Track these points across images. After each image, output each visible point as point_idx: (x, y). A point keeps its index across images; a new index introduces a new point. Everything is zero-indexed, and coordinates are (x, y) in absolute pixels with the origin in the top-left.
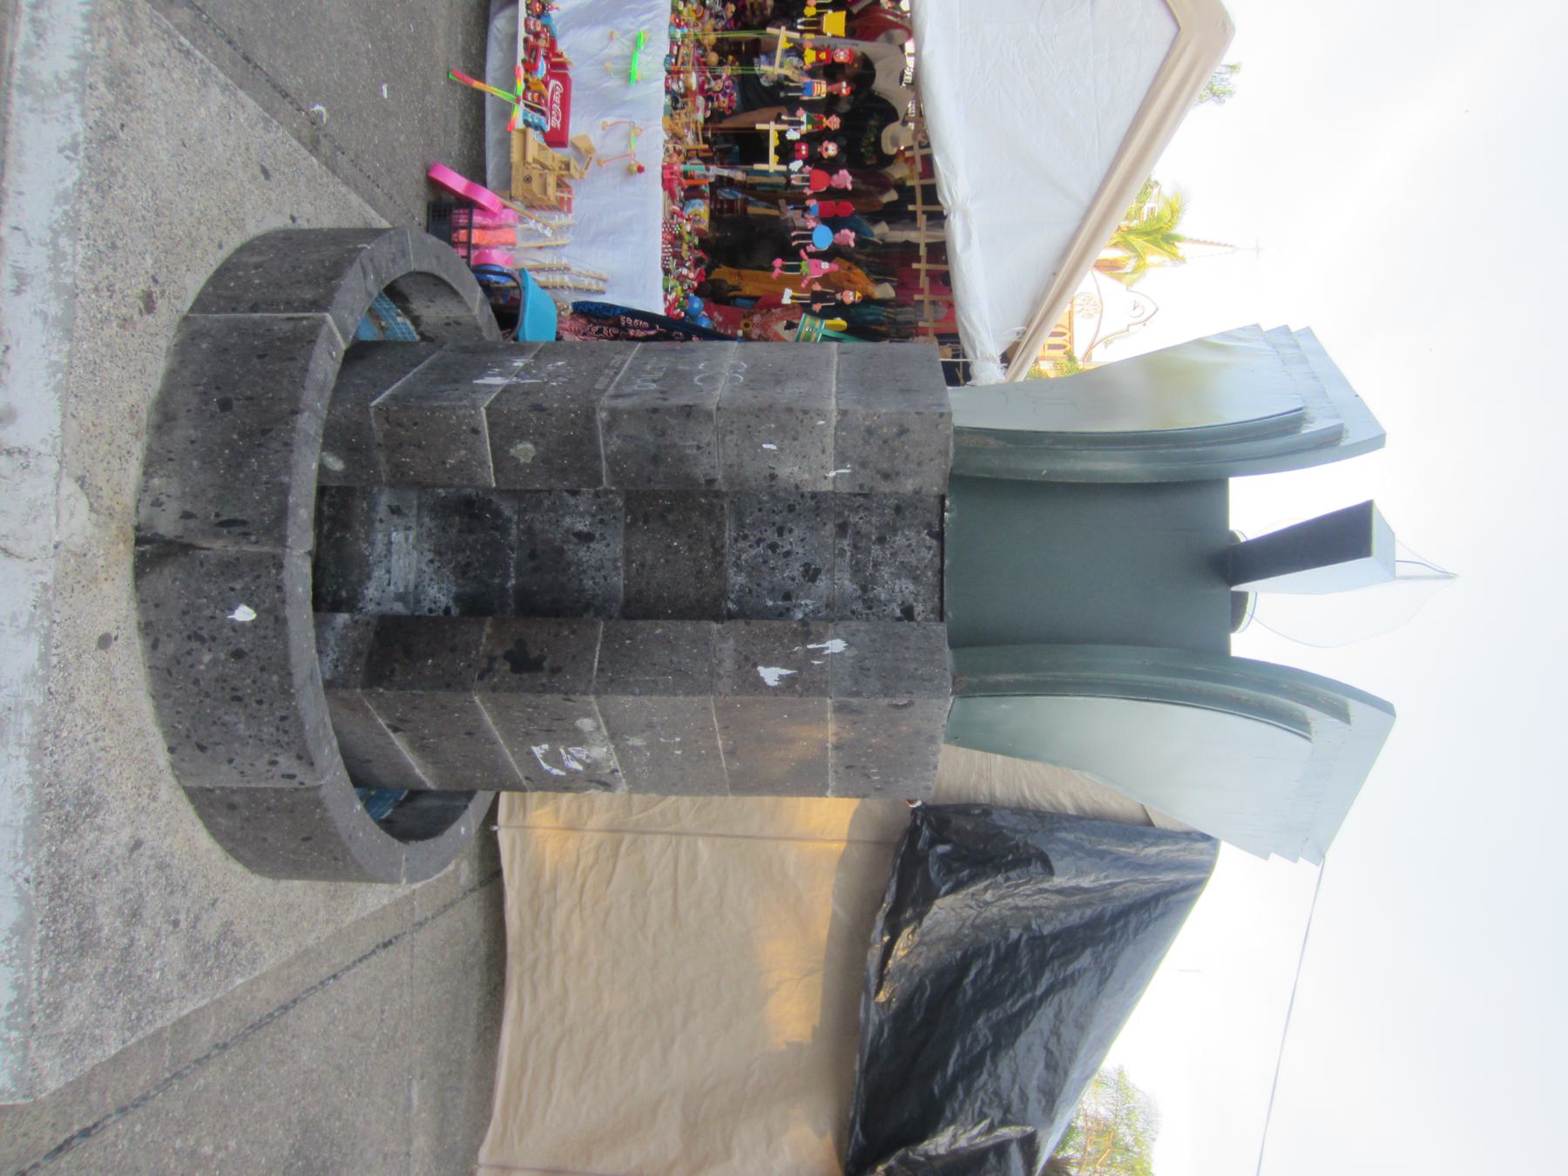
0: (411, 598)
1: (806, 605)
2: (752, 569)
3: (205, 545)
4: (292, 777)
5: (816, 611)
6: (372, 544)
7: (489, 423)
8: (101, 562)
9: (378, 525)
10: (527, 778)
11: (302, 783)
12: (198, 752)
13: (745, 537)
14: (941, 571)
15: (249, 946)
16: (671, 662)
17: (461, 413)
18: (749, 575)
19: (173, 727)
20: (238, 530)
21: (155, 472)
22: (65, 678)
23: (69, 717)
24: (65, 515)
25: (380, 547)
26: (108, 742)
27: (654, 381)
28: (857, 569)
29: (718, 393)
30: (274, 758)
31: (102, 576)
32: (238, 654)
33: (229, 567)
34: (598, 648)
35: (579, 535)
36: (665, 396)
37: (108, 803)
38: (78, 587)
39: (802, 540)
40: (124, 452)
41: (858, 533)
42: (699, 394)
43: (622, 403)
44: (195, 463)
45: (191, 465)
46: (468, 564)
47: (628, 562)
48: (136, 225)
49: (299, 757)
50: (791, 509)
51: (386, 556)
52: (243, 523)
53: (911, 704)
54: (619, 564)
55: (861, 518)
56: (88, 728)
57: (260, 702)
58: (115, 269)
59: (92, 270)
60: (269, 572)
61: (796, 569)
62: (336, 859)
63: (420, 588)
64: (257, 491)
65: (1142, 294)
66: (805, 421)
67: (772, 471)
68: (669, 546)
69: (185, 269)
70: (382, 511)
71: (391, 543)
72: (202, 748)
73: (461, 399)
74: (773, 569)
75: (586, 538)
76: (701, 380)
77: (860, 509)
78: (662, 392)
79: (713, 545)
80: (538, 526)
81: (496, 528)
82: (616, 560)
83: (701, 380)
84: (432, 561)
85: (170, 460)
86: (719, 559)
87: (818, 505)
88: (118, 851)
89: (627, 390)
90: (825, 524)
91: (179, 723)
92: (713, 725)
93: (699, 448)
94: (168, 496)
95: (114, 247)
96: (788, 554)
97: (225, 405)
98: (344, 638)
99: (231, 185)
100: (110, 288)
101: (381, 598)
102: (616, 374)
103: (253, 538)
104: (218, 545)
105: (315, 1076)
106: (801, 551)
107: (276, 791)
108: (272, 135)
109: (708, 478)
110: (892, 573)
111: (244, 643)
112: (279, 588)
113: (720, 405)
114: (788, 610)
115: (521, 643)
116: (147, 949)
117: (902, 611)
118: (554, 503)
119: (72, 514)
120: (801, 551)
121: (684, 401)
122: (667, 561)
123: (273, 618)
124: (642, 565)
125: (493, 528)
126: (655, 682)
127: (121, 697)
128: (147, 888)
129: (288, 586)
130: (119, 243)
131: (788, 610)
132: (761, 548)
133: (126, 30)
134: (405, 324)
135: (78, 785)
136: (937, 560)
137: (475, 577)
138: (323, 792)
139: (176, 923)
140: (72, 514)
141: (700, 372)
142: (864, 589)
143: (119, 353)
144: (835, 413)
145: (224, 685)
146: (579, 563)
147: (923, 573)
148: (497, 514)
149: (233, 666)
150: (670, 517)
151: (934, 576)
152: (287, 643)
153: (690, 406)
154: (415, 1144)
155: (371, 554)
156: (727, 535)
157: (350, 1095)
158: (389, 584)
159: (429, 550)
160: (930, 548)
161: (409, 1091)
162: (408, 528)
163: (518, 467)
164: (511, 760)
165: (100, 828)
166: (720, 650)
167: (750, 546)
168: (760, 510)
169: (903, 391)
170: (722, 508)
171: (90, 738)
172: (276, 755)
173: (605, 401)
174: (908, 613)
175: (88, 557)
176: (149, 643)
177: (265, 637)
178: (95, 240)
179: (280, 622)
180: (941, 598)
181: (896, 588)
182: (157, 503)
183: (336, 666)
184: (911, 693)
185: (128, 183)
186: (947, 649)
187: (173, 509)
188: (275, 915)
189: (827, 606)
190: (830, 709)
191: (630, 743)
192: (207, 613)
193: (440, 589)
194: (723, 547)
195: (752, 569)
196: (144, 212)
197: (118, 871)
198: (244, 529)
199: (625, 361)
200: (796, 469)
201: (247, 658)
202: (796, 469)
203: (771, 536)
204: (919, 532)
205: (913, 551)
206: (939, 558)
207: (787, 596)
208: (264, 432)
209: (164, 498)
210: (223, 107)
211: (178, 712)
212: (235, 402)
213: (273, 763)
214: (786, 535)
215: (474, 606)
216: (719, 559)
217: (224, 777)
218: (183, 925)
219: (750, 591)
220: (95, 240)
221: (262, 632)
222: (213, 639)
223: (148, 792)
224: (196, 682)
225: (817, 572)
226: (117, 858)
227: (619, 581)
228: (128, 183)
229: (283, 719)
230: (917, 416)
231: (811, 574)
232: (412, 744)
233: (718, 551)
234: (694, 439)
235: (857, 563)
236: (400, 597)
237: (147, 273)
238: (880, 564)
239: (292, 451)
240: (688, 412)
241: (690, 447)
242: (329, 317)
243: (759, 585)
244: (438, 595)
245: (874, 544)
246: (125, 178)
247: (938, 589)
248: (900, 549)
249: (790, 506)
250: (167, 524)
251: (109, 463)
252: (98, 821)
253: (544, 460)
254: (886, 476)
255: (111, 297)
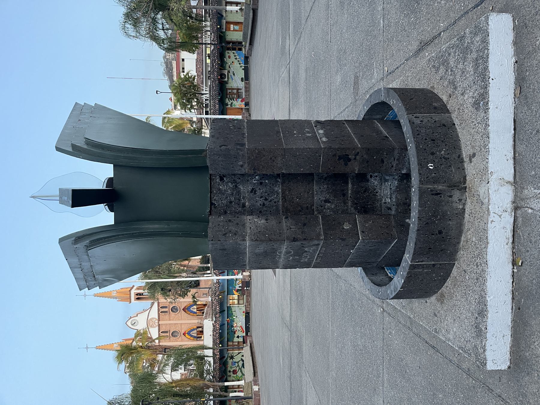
0: (383, 181)
1: (255, 181)
2: (273, 192)
3: (444, 187)
4: (415, 117)
5: (252, 179)
6: (396, 197)
7: (359, 235)
8: (476, 180)
9: (395, 204)
10: (344, 124)
11: (413, 115)
12: (446, 124)
13: (275, 202)
14: (211, 192)
15: (431, 66)
16: (298, 159)
17: (368, 237)
18: (274, 190)
19: (453, 131)
20: (434, 192)
21: (462, 210)
22: (484, 142)
23: (483, 131)
24: (486, 192)
25: (394, 197)
26: (471, 124)
27: (306, 251)
28: (239, 193)
29: (285, 247)
30: (421, 123)
31: (475, 176)
32: (433, 154)
33: (436, 181)
34: (321, 163)
35: (329, 202)
36: (302, 245)
37: (471, 106)
38: (482, 171)
39: (257, 202)
40: (471, 215)
41: (238, 204)
42: (291, 246)
43: (316, 242)
44: (449, 213)
45: (450, 213)
46: (365, 192)
47: (313, 193)
48: (471, 288)
49: (413, 123)
50: (261, 212)
51: (392, 194)
52: (433, 194)
53: (220, 146)
54: (316, 193)
55: (238, 209)
56: (477, 128)
57: (426, 139)
58: (476, 272)
59: (483, 270)
60: (424, 179)
61: (258, 193)
62: (403, 94)
63: (380, 184)
64: (429, 205)
65: (129, 327)
66: (256, 237)
67: (267, 221)
68: (300, 199)
69: (457, 278)
70: (394, 208)
71: (390, 198)
72: (444, 125)
73: (368, 242)
74: (266, 192)
75: (327, 201)
76: (291, 252)
77: (238, 212)
78: (303, 247)
79: (286, 199)
80: (342, 204)
81: (356, 204)
82: (317, 194)
83: (291, 252)
84: (377, 193)
85: (457, 214)
86: (283, 195)
87: (251, 213)
88: (468, 91)
89: (314, 248)
90: (249, 207)
91: (451, 133)
92: (284, 140)
93: (291, 228)
94: (457, 202)
95: (477, 279)
96: (261, 197)
97: (440, 232)
98: (403, 165)
99: (445, 308)
100: (477, 266)
101: (393, 180)
102: (318, 254)
103: (429, 190)
104: (440, 187)
105: (412, 28)
106: (257, 198)
107: (421, 113)
108: (434, 328)
109: (288, 219)
110: (227, 192)
111: (431, 157)
112: (420, 174)
113: (284, 242)
114: (261, 179)
115: (346, 164)
116: (459, 62)
117: (224, 179)
118: (337, 212)
119: (484, 193)
120: (257, 198)
121: (296, 243)
122: (300, 194)
123: (422, 165)
124: (308, 193)
125: (357, 204)
126: (303, 152)
127: (469, 139)
128: (460, 81)
129: (418, 175)
130: (476, 281)
131: (261, 179)
132: (270, 199)
133: (478, 349)
134: (390, 274)
135: (480, 110)
136: (212, 196)
137: (362, 188)
138: (406, 113)
139: (451, 71)
140: (484, 193)
141: (291, 256)
142: (236, 186)
143: (474, 246)
144: (247, 240)
145: (437, 144)
146: (328, 193)
147: (217, 192)
148: (356, 209)
149: (434, 150)
150: (300, 208)
151: (213, 191)
152: (417, 158)
153: (294, 241)
154: (381, 7)
155: (397, 194)
156: (281, 204)
157: (402, 22)
158: (390, 185)
159: (377, 196)
160: (215, 200)
161: (383, 24)
162: (385, 203)
163: (349, 221)
164: (349, 129)
165: (473, 97)
166: (282, 164)
167: (273, 199)
168: (271, 211)
169: (225, 250)
170: (283, 212)
171: (477, 125)
172: (421, 124)
173: (322, 243)
174: (222, 179)
175: (479, 181)
176: (461, 157)
177: (425, 159)
178: (482, 280)
179: (420, 164)
180: (211, 184)
181: (226, 187)
182: (460, 200)
183: (405, 155)
184: (220, 150)
185: (474, 300)
186: (208, 164)
187: (455, 198)
188: (423, 77)
189: (248, 181)
190: (246, 145)
191: (311, 134)
192: (443, 166)
193: (374, 183)
194: (282, 199)
195: (273, 192)
196: (469, 292)
197: (468, 85)
198: (432, 192)
199: (316, 260)
200: (259, 222)
201: (430, 153)
202: (259, 222)
203: (267, 203)
204: (219, 205)
205: (220, 199)
206: (212, 197)
207: (261, 183)
208: (427, 223)
209: (458, 202)
210: (449, 333)
211: (452, 136)
212: (437, 233)
213: (421, 121)
214: (262, 204)
215: (362, 177)
216: (283, 195)
217: (436, 117)
218: (449, 70)
219: (273, 185)
220: (482, 280)
221: (425, 160)
222: (441, 158)
223: (461, 111)
224: (446, 145)
225: (251, 192)
226: (468, 89)
227: (315, 187)
228: (474, 300)
229: (418, 134)
230: (220, 240)
231: (253, 191)
232: (381, 133)
233: (284, 197)
234: (292, 231)
235: (239, 195)
236: (386, 181)
237: (467, 273)
238: (231, 194)
239: (418, 217)
240: (295, 240)
241: (293, 228)
242: (410, 263)
243: (270, 187)
244: (374, 182)
245: (233, 201)
246: (475, 302)
247: (212, 187)
248: (224, 199)
249: (261, 213)
250: (456, 194)
251: (475, 211)
252: (474, 100)
253: (341, 224)
254: (230, 221)
255: (477, 263)
